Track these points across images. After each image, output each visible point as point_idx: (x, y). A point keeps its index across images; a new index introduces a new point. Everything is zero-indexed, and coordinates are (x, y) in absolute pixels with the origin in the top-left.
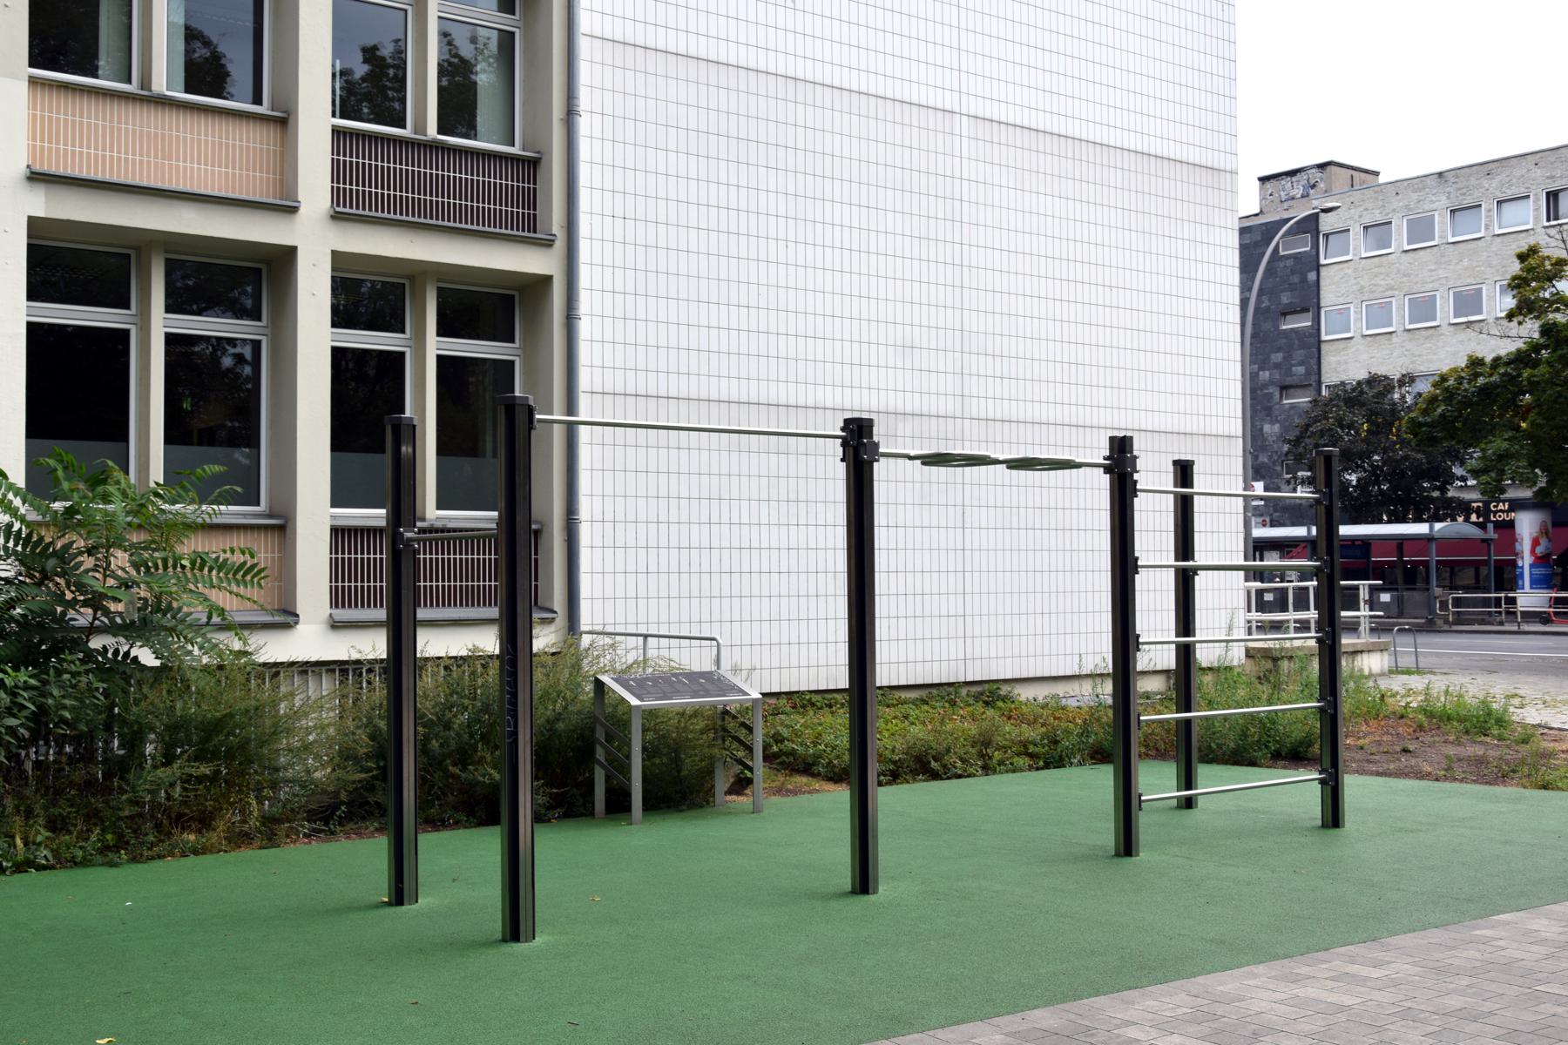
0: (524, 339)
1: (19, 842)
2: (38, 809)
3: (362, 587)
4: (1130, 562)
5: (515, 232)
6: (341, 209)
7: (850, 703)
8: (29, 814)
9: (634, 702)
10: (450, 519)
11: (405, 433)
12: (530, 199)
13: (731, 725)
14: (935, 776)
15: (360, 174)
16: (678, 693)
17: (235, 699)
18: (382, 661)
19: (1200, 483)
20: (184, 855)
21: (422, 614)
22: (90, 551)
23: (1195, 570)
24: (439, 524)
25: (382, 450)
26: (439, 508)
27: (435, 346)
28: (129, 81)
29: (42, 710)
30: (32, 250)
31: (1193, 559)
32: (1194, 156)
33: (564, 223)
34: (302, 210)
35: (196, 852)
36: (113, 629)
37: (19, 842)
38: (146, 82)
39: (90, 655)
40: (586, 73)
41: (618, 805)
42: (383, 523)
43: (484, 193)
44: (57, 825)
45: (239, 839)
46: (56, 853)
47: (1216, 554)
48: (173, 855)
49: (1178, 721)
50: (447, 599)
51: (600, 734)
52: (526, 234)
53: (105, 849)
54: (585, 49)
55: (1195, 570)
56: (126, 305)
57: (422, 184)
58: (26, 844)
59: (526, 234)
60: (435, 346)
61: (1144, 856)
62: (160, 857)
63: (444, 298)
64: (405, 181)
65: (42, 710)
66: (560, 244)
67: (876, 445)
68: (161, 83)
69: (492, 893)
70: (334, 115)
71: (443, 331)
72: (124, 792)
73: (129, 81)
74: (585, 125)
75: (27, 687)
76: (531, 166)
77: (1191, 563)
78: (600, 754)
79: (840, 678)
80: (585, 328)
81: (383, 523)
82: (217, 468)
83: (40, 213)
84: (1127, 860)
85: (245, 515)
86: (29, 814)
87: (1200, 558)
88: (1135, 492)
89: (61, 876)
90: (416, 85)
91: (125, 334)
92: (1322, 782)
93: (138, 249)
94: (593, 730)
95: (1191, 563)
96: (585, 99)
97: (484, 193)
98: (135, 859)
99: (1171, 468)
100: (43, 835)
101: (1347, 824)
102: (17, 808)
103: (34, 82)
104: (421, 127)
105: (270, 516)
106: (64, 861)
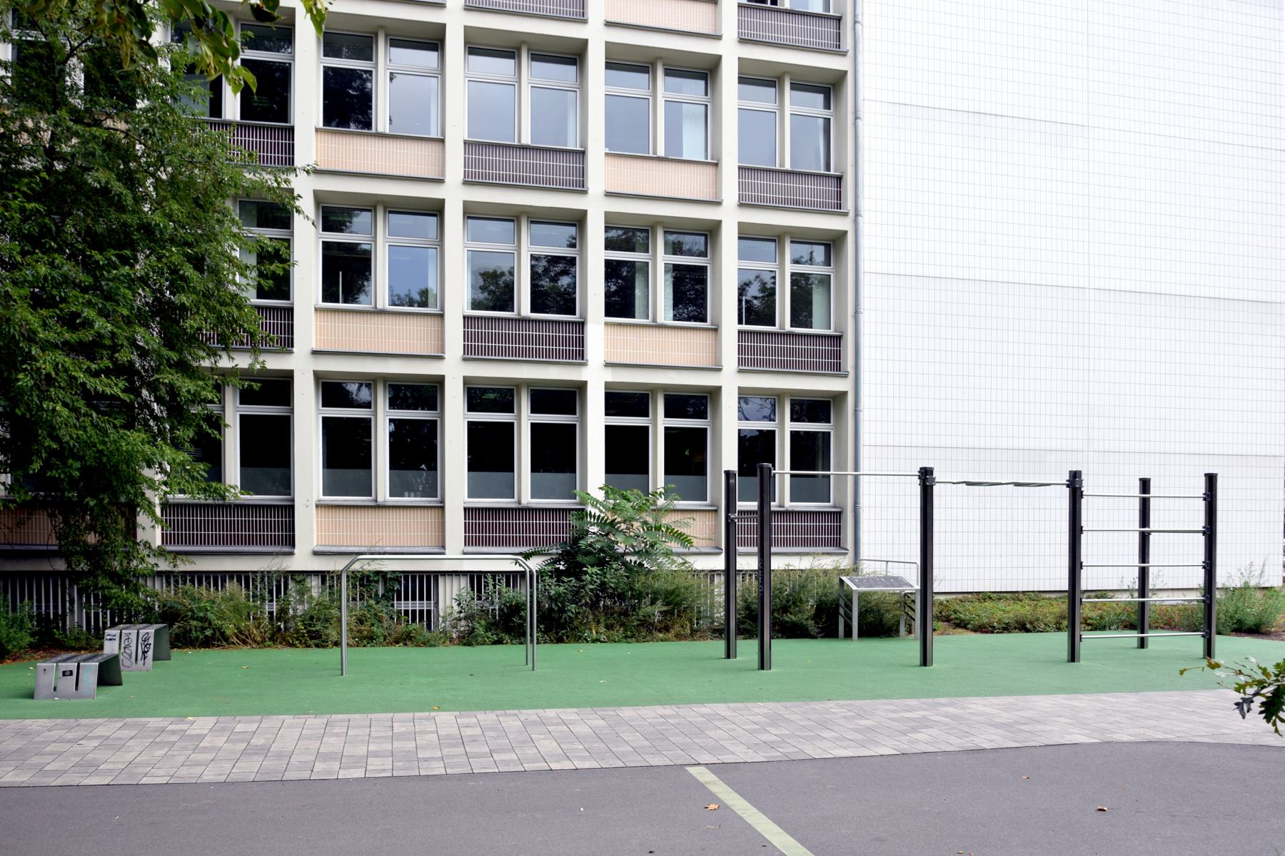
0: (836, 421)
1: (594, 632)
2: (602, 620)
3: (197, 534)
4: (1078, 528)
5: (829, 372)
6: (741, 368)
7: (1069, 596)
8: (598, 622)
9: (854, 588)
10: (798, 507)
11: (731, 476)
12: (838, 355)
13: (909, 602)
14: (1028, 631)
15: (752, 350)
16: (878, 585)
17: (680, 582)
18: (755, 571)
19: (1154, 491)
20: (657, 641)
21: (774, 549)
22: (624, 522)
23: (1149, 533)
24: (790, 509)
25: (756, 476)
26: (791, 501)
27: (790, 426)
28: (648, 318)
29: (603, 583)
30: (607, 394)
31: (1149, 527)
32: (1252, 296)
33: (854, 366)
34: (724, 370)
35: (662, 641)
36: (635, 553)
37: (594, 632)
38: (654, 320)
39: (625, 564)
40: (865, 291)
41: (848, 634)
42: (756, 509)
43: (813, 354)
44: (608, 627)
45: (679, 637)
46: (608, 637)
47: (1171, 523)
48: (653, 641)
49: (1139, 602)
50: (786, 543)
51: (842, 602)
52: (835, 372)
53: (626, 637)
54: (865, 280)
55: (1149, 533)
56: (647, 415)
57: (782, 352)
58: (597, 633)
59: (835, 372)
60: (790, 426)
61: (1082, 663)
62: (648, 641)
63: (793, 404)
64: (774, 351)
65: (603, 583)
66: (851, 375)
67: (934, 479)
68: (661, 319)
69: (755, 657)
70: (740, 322)
71: (792, 420)
72: (633, 615)
73: (648, 318)
74: (865, 317)
75: (597, 574)
76: (837, 339)
77: (1146, 529)
78: (841, 611)
79: (1064, 585)
80: (865, 416)
81: (756, 509)
82: (673, 486)
83: (610, 380)
84: (1072, 663)
85: (700, 505)
86: (598, 622)
87: (1153, 526)
88: (1082, 496)
89: (609, 645)
90: (780, 306)
91: (647, 428)
92: (1203, 636)
93: (652, 391)
94: (838, 600)
95: (1146, 529)
96: (865, 304)
97: (813, 354)
98: (638, 641)
99: (1138, 482)
100: (603, 630)
101: (1149, 647)
102: (594, 619)
103: (606, 324)
104: (782, 326)
105: (712, 506)
106: (611, 640)
